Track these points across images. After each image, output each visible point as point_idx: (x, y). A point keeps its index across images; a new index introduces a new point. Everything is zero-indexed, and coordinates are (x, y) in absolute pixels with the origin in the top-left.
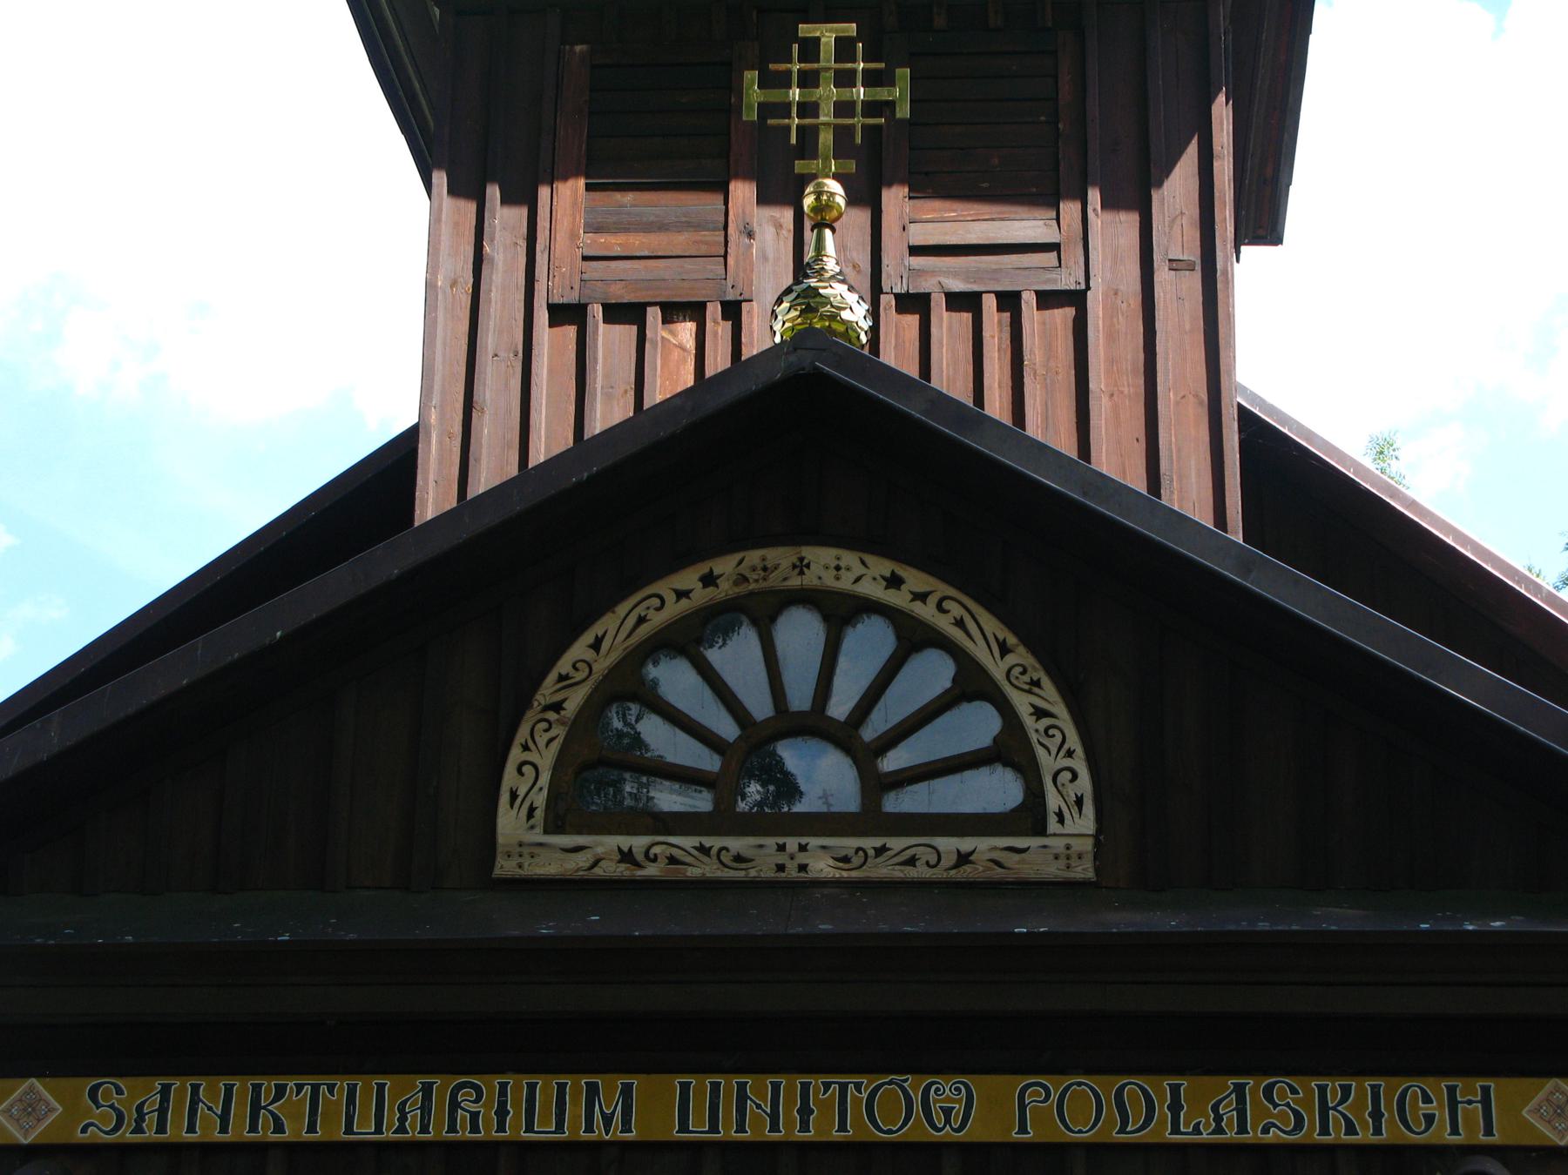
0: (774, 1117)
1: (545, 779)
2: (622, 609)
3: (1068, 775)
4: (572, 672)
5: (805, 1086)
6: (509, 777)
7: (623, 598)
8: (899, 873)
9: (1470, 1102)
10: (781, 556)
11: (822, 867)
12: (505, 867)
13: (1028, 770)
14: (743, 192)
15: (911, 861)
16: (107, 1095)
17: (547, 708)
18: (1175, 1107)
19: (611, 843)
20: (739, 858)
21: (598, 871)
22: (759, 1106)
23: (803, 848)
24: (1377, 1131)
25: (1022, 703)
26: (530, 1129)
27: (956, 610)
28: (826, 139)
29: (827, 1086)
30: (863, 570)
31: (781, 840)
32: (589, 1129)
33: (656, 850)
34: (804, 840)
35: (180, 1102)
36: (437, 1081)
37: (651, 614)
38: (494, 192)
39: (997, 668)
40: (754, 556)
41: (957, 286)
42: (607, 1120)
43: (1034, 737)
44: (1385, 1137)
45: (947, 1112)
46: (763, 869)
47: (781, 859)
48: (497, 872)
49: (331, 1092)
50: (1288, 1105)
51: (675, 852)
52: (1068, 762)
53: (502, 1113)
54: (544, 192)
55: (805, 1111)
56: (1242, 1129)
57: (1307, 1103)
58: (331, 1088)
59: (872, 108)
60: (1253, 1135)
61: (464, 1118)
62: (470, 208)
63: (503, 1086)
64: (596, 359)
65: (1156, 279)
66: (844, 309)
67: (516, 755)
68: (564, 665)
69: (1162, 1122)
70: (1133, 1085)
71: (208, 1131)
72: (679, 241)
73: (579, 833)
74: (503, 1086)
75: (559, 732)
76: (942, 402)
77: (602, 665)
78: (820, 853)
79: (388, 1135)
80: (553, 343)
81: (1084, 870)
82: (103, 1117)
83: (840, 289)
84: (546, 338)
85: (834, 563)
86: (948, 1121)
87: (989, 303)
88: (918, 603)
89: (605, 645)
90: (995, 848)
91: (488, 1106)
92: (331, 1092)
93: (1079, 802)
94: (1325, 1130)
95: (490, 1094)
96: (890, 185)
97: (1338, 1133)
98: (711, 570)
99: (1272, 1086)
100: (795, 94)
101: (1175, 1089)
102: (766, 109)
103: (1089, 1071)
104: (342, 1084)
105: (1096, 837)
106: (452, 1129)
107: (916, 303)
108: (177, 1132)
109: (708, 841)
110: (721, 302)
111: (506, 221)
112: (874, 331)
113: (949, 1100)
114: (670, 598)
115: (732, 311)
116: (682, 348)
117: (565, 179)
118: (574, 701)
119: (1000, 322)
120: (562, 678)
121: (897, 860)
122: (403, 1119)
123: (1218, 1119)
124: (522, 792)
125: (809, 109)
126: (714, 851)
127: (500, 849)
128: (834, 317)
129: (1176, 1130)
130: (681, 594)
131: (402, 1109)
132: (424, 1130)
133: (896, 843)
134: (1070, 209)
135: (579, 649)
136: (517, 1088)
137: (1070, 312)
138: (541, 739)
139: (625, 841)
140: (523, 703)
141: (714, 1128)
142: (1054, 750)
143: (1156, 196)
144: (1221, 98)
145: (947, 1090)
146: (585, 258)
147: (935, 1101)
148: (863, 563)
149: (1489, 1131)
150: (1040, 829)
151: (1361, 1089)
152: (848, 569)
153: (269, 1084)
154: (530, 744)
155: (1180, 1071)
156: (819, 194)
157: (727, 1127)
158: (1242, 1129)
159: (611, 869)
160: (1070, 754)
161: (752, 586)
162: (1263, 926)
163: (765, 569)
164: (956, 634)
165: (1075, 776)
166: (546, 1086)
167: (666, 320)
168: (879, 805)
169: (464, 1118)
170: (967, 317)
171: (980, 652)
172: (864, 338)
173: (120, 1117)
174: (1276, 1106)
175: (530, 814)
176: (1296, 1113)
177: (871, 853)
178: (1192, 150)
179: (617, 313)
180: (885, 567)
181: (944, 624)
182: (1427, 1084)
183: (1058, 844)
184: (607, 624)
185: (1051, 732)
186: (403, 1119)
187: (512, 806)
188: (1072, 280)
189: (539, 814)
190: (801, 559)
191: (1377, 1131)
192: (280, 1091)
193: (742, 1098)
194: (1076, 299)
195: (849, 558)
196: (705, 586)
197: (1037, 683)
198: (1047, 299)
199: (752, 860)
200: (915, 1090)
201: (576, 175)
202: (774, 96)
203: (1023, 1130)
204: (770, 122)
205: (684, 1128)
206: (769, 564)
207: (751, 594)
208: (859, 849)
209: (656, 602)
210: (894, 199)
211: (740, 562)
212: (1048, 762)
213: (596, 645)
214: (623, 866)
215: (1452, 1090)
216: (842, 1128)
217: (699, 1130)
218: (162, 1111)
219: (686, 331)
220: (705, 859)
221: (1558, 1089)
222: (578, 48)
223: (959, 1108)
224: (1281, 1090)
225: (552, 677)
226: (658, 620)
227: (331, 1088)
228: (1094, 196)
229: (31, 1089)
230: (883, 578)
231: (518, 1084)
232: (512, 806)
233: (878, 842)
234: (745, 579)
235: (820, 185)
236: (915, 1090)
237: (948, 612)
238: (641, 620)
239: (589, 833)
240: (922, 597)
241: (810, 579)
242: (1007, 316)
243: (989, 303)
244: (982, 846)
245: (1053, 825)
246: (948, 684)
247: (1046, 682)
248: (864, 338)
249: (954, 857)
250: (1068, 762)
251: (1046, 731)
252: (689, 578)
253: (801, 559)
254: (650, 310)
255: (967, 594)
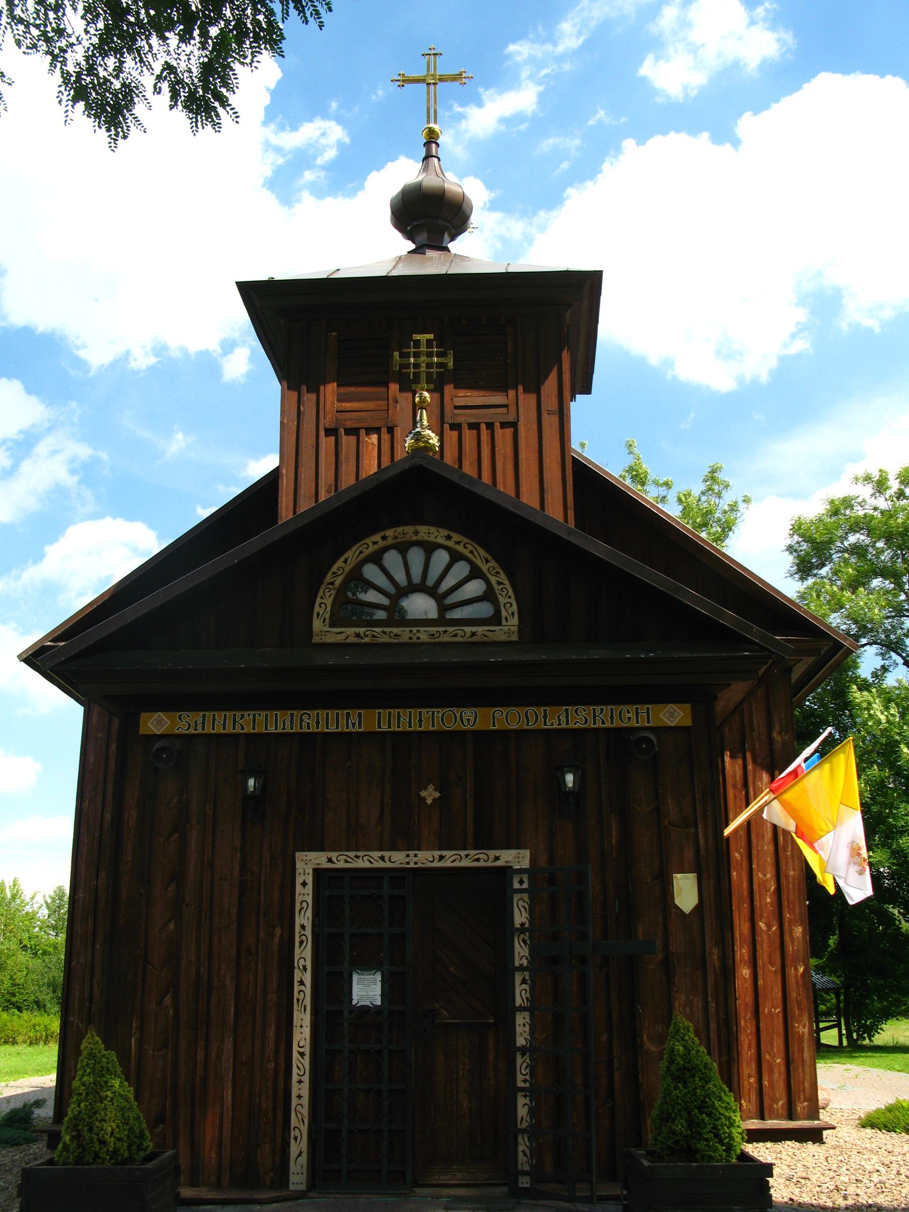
0: (410, 723)
1: (329, 609)
2: (354, 549)
3: (509, 605)
4: (337, 571)
5: (420, 712)
6: (317, 608)
7: (353, 545)
8: (451, 640)
9: (643, 713)
10: (409, 529)
11: (424, 638)
12: (316, 639)
13: (495, 602)
14: (394, 387)
15: (456, 635)
16: (185, 718)
17: (329, 584)
18: (545, 717)
19: (352, 630)
20: (396, 635)
21: (348, 640)
22: (405, 719)
23: (418, 631)
24: (612, 723)
25: (493, 580)
26: (327, 728)
27: (470, 547)
28: (423, 377)
29: (428, 712)
30: (437, 534)
31: (410, 629)
32: (347, 728)
33: (368, 633)
34: (418, 629)
35: (209, 721)
36: (295, 712)
37: (364, 550)
38: (304, 388)
39: (484, 568)
40: (400, 529)
41: (472, 420)
42: (354, 725)
43: (497, 592)
44: (614, 725)
45: (468, 720)
46: (405, 639)
47: (411, 635)
48: (313, 641)
49: (260, 717)
50: (583, 715)
51: (374, 633)
52: (509, 600)
53: (318, 723)
54: (322, 388)
55: (420, 721)
56: (567, 724)
57: (589, 714)
58: (259, 715)
59: (439, 365)
60: (571, 725)
61: (305, 724)
62: (296, 394)
63: (318, 714)
64: (342, 449)
65: (543, 417)
66: (430, 439)
67: (318, 600)
68: (334, 569)
69: (541, 722)
70: (531, 710)
71: (219, 730)
72: (370, 405)
73: (341, 627)
74: (318, 714)
75: (334, 592)
76: (464, 476)
77: (348, 568)
78: (424, 633)
79: (280, 730)
80: (327, 443)
81: (515, 637)
82: (184, 725)
83: (429, 432)
84: (324, 441)
85: (427, 531)
86: (469, 723)
87: (483, 426)
88: (457, 545)
89: (349, 562)
90: (484, 630)
91: (313, 721)
92: (260, 717)
93: (513, 614)
94: (595, 724)
95: (314, 716)
96: (446, 384)
97: (599, 724)
98: (385, 535)
99: (181, 715)
100: (412, 360)
101: (545, 711)
102: (402, 366)
103: (516, 706)
104: (263, 714)
105: (519, 626)
106: (301, 728)
107: (456, 427)
108: (209, 730)
109: (385, 629)
110: (387, 428)
111: (309, 399)
112: (442, 447)
113: (469, 716)
114: (371, 544)
115: (391, 430)
116: (373, 444)
117: (329, 383)
118: (338, 581)
119: (487, 433)
120: (334, 573)
121: (451, 635)
122: (284, 725)
123: (559, 720)
124: (321, 613)
125: (417, 366)
126: (388, 633)
127: (314, 633)
128: (427, 442)
129: (545, 724)
130: (375, 543)
131: (284, 721)
132: (292, 728)
133: (450, 629)
134: (512, 393)
135: (340, 563)
136: (323, 714)
137: (512, 430)
138: (327, 594)
139: (357, 630)
140: (320, 582)
141: (389, 727)
142: (504, 596)
143: (542, 388)
144: (565, 351)
145: (469, 713)
146: (337, 412)
147: (465, 717)
148: (438, 531)
149: (648, 722)
150: (499, 623)
151: (607, 709)
152: (433, 533)
153: (239, 714)
154: (324, 597)
155: (547, 705)
156: (421, 397)
157: (394, 726)
158: (567, 724)
159: (352, 640)
160: (510, 597)
161: (399, 540)
162: (574, 657)
163: (404, 534)
164: (470, 556)
165: (511, 605)
166: (332, 714)
167: (367, 434)
168: (444, 617)
169: (305, 724)
170: (475, 432)
171: (478, 562)
172: (437, 449)
173: (189, 725)
174: (579, 715)
175: (324, 621)
176: (585, 718)
177: (442, 633)
178: (554, 372)
179: (350, 431)
180: (445, 532)
181: (466, 552)
182: (628, 707)
183: (506, 629)
184: (349, 554)
185: (503, 590)
186: (284, 725)
187: (318, 618)
188: (512, 418)
189: (327, 621)
190: (416, 530)
191: (612, 723)
192: (243, 716)
193: (399, 717)
194: (514, 425)
195: (433, 530)
196: (383, 540)
197: (498, 573)
198: (504, 425)
199: (400, 636)
200: (457, 713)
201: (333, 382)
202: (404, 361)
203: (494, 726)
204: (403, 370)
205: (379, 727)
206: (405, 532)
207: (399, 542)
208: (438, 631)
209: (366, 546)
210: (449, 389)
211: (395, 532)
212: (502, 600)
213: (345, 562)
214: (356, 639)
215: (637, 709)
216: (433, 726)
217: (384, 728)
218: (203, 723)
219: (374, 438)
220: (385, 635)
221: (671, 707)
222: (333, 334)
223: (472, 719)
224: (581, 711)
225: (330, 573)
226: (367, 552)
227: (259, 715)
228: (520, 388)
229: (159, 716)
230: (445, 536)
231: (322, 713)
232: (318, 618)
233: (444, 629)
234: (396, 537)
235: (421, 394)
236: (457, 713)
237: (467, 548)
238: (361, 552)
239: (345, 627)
240: (458, 543)
241: (419, 537)
242: (489, 431)
243: (483, 426)
244: (479, 629)
245: (504, 622)
246: (468, 573)
247: (501, 572)
248: (437, 449)
249: (470, 633)
250: (509, 600)
251: (502, 589)
252: (377, 537)
253: (416, 530)
254: (361, 430)
255: (474, 541)
